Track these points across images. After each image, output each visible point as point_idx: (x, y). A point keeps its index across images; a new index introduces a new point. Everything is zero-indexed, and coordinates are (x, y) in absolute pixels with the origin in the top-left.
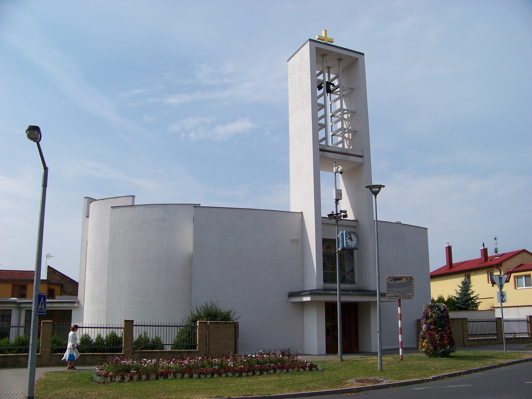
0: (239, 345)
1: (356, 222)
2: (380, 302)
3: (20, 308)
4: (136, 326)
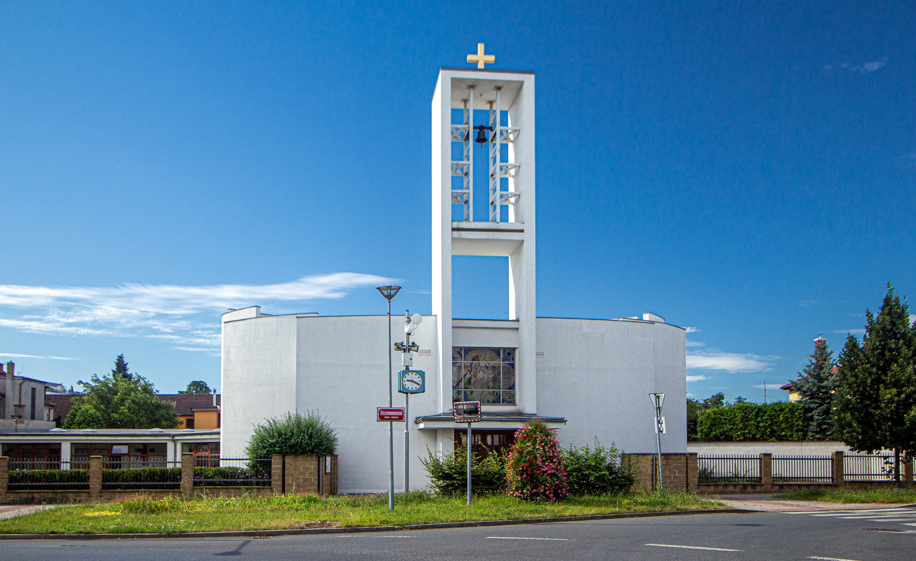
3: (175, 442)
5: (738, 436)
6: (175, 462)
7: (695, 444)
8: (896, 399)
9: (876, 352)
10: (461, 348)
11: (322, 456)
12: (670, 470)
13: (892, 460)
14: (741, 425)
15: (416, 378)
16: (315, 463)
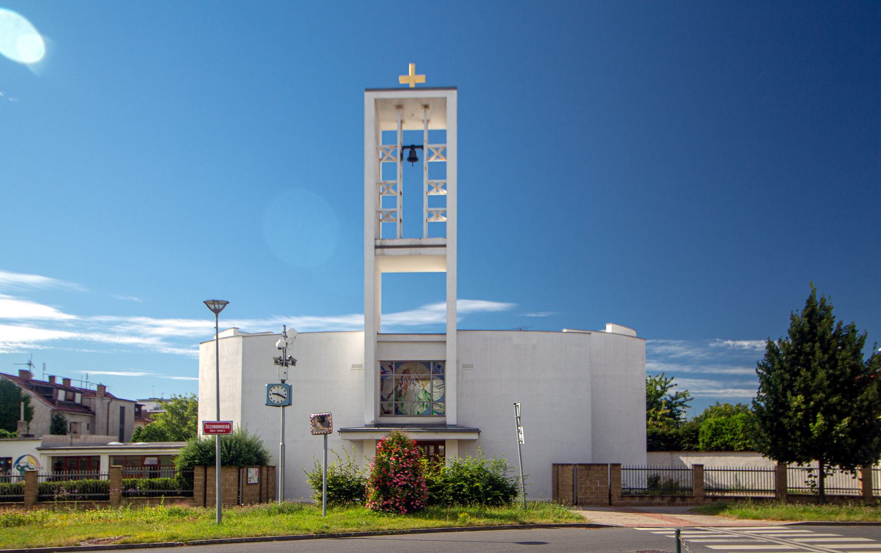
5: (739, 446)
7: (697, 454)
8: (803, 407)
9: (790, 357)
10: (392, 362)
11: (242, 467)
12: (591, 481)
13: (816, 473)
14: (742, 436)
16: (235, 475)
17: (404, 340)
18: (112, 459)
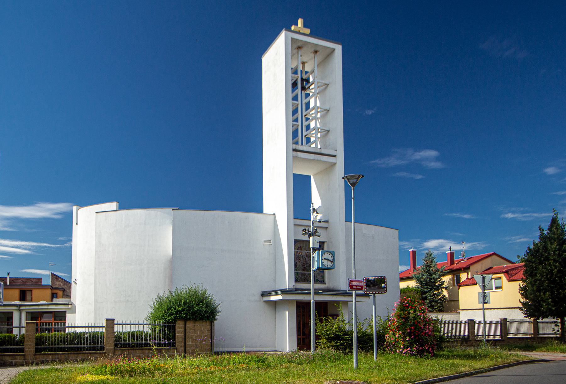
0: (215, 342)
1: (327, 223)
2: (356, 301)
3: (20, 311)
4: (117, 324)
6: (20, 327)
15: (329, 257)
17: (301, 224)
18: (29, 316)
